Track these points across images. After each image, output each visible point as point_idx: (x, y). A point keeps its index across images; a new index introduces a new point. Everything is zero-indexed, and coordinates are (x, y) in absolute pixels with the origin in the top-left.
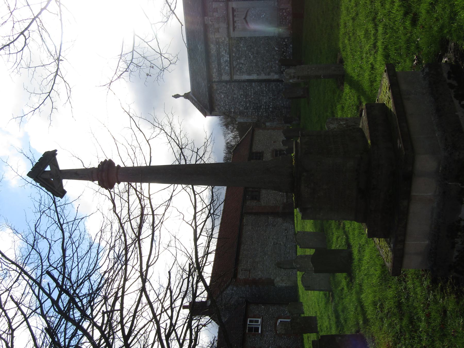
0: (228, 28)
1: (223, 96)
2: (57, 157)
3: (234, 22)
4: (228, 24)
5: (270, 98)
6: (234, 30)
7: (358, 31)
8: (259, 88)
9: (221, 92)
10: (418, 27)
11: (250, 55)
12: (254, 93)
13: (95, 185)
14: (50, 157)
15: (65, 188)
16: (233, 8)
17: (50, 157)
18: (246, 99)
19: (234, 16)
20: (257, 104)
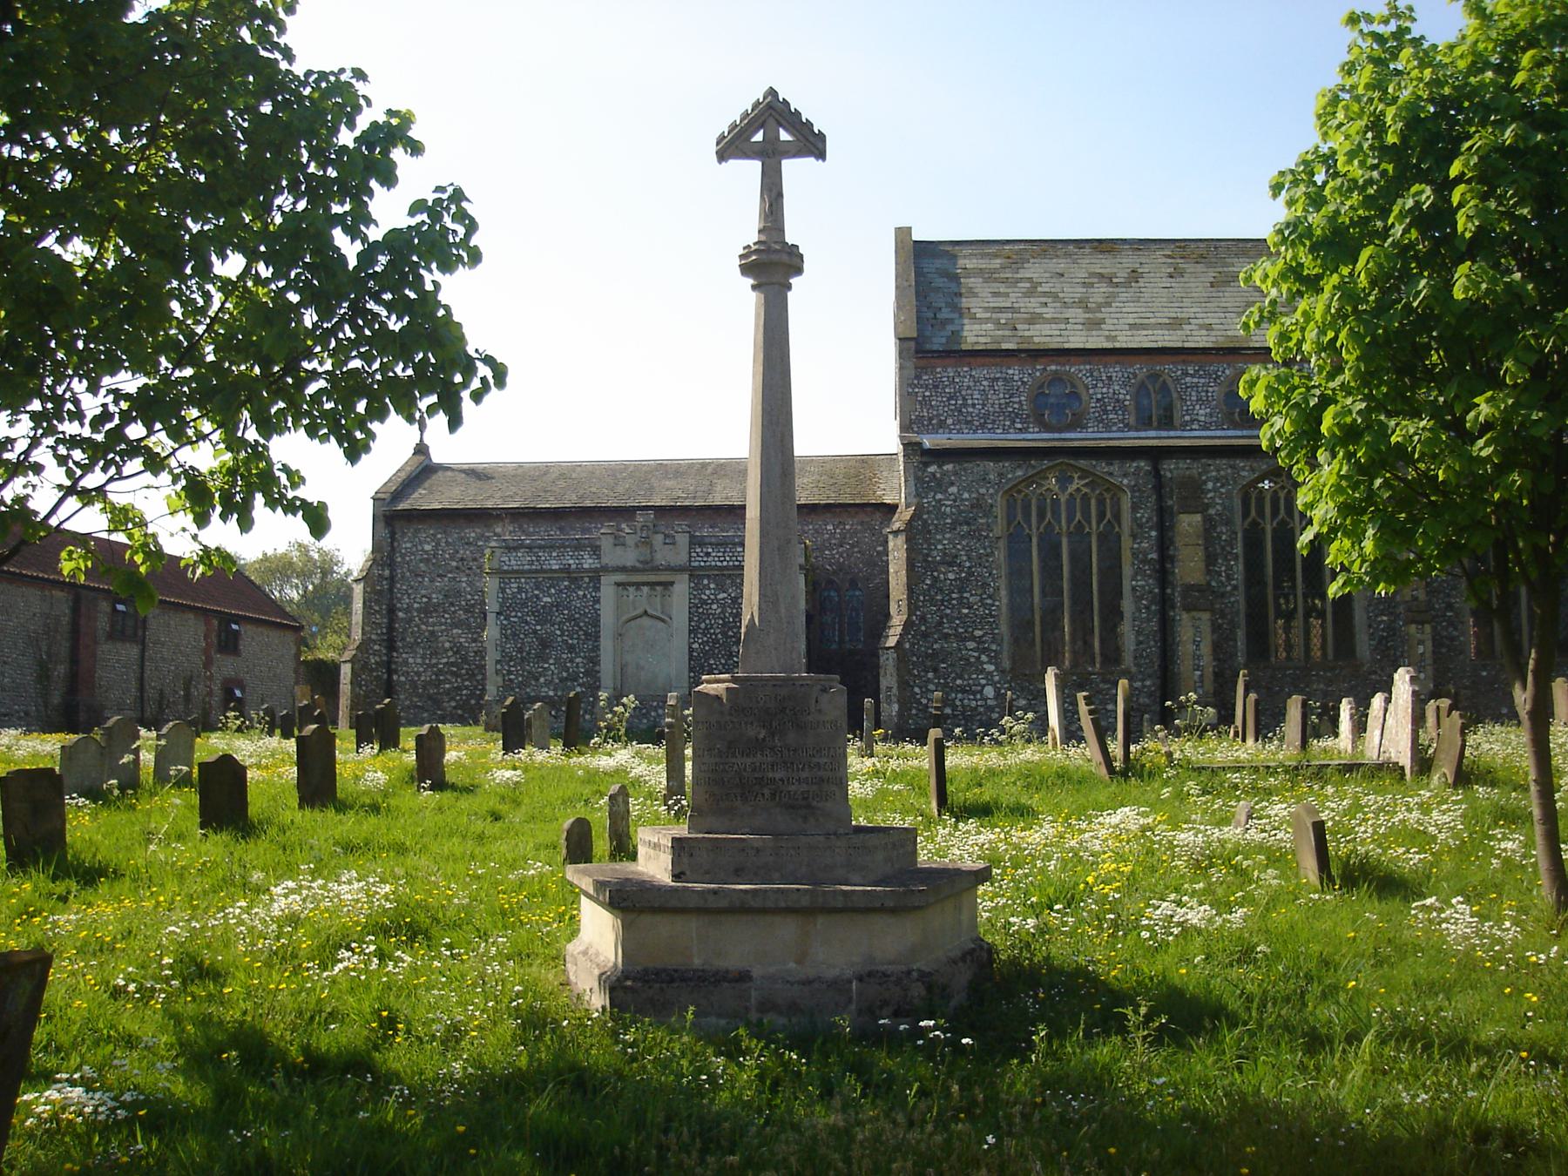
0: (623, 569)
1: (427, 547)
2: (812, 160)
3: (638, 585)
4: (634, 570)
5: (418, 674)
6: (618, 584)
7: (953, 1003)
8: (447, 645)
9: (438, 544)
10: (39, 935)
11: (1496, 747)
12: (432, 633)
13: (751, 236)
14: (812, 144)
15: (731, 162)
16: (672, 583)
17: (812, 144)
18: (418, 610)
19: (652, 585)
20: (403, 639)
